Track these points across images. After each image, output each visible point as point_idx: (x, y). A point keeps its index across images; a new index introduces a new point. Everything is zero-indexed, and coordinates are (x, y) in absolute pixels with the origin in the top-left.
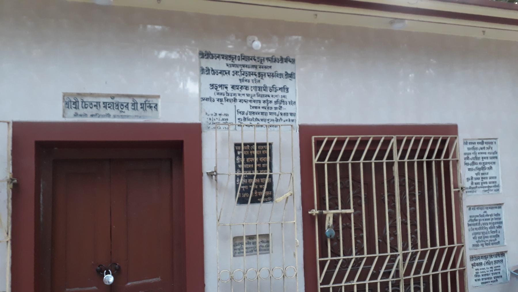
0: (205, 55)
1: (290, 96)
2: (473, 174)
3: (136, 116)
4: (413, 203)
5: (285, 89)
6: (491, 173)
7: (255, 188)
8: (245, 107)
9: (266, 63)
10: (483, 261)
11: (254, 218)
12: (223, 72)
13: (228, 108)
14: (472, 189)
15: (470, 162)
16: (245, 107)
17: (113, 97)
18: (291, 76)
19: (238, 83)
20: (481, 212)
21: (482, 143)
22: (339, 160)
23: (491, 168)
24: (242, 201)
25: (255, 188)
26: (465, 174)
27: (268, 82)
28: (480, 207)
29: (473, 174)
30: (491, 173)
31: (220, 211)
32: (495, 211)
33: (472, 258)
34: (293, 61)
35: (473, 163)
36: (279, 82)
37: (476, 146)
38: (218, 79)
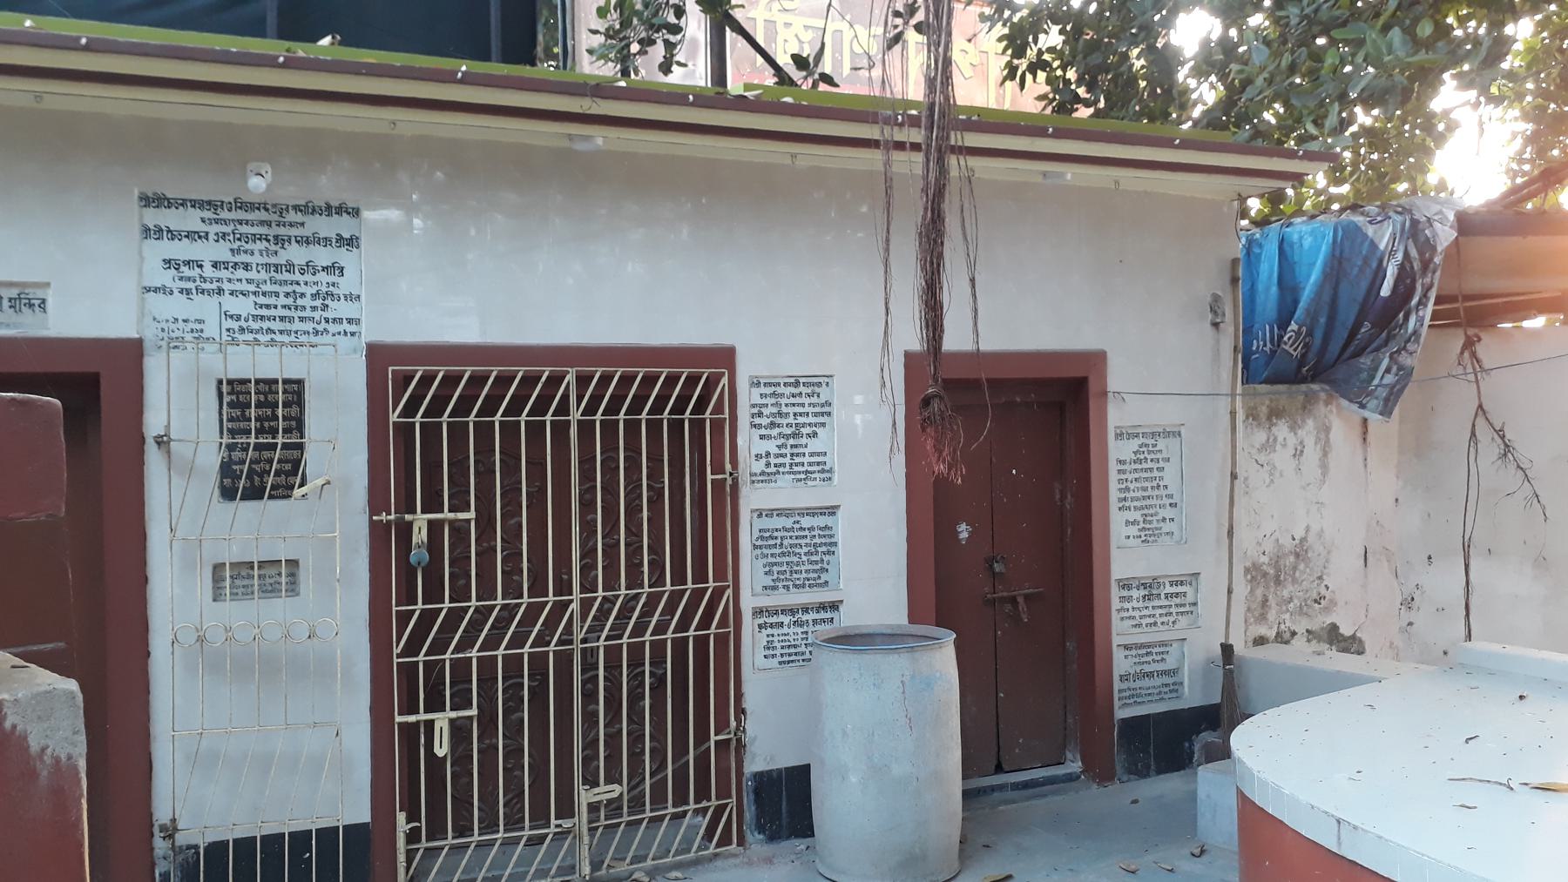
2: (771, 446)
5: (335, 269)
6: (814, 445)
8: (244, 306)
9: (292, 216)
10: (786, 619)
11: (255, 528)
12: (191, 235)
13: (206, 308)
14: (767, 477)
15: (765, 421)
16: (244, 306)
18: (351, 242)
19: (226, 256)
20: (788, 523)
21: (796, 384)
23: (815, 434)
26: (751, 444)
27: (296, 254)
28: (782, 512)
29: (771, 446)
31: (184, 519)
33: (758, 612)
34: (356, 212)
35: (773, 425)
36: (322, 256)
38: (181, 250)
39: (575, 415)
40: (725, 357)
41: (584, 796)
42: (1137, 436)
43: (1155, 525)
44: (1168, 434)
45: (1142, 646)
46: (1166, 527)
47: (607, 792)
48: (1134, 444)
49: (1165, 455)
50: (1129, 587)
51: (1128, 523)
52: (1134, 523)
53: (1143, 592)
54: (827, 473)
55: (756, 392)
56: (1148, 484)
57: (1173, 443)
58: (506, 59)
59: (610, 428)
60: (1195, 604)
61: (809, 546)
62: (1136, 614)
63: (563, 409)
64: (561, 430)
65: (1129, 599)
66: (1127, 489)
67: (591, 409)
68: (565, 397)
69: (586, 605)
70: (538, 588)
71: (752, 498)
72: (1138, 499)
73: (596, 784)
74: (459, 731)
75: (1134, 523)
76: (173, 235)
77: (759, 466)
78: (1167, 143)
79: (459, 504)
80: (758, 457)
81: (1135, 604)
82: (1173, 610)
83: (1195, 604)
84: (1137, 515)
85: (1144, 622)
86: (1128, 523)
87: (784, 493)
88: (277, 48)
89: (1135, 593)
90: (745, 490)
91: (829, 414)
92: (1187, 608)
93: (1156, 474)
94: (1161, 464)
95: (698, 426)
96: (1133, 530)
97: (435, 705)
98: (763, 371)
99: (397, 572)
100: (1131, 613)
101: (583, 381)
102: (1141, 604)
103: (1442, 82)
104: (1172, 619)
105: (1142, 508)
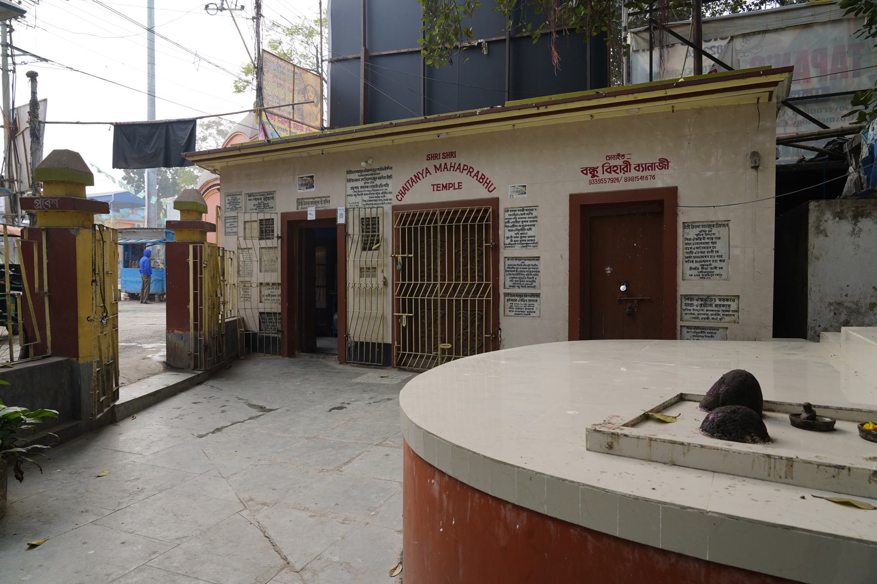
0: (349, 172)
1: (390, 189)
2: (513, 234)
3: (870, 459)
4: (443, 246)
5: (387, 185)
6: (530, 233)
7: (370, 242)
8: (366, 198)
9: (377, 172)
10: (518, 299)
11: (370, 258)
12: (357, 180)
13: (359, 199)
14: (511, 245)
15: (510, 224)
16: (366, 198)
17: (313, 198)
18: (390, 177)
19: (363, 185)
20: (520, 263)
21: (523, 210)
22: (414, 225)
23: (530, 229)
24: (364, 249)
25: (370, 242)
26: (505, 233)
27: (378, 182)
28: (517, 258)
29: (513, 234)
30: (530, 233)
31: (355, 258)
32: (533, 262)
33: (506, 295)
34: (391, 168)
35: (513, 226)
36: (384, 182)
37: (517, 212)
38: (354, 184)
39: (440, 224)
41: (441, 346)
42: (699, 226)
43: (709, 270)
44: (719, 225)
45: (698, 328)
46: (716, 272)
47: (448, 346)
49: (717, 236)
50: (692, 299)
51: (691, 268)
52: (695, 269)
54: (536, 245)
55: (507, 214)
56: (706, 250)
58: (365, 123)
59: (450, 228)
60: (737, 311)
61: (528, 271)
62: (696, 312)
63: (436, 222)
64: (435, 228)
65: (692, 305)
66: (692, 252)
67: (444, 222)
68: (436, 219)
69: (442, 285)
71: (504, 253)
72: (698, 257)
73: (444, 342)
74: (409, 319)
75: (695, 269)
76: (353, 180)
77: (508, 241)
78: (614, 94)
80: (508, 238)
81: (695, 308)
82: (720, 313)
83: (737, 311)
84: (698, 265)
85: (700, 317)
86: (691, 268)
87: (517, 251)
89: (695, 303)
90: (502, 250)
91: (273, 198)
92: (731, 313)
93: (710, 245)
94: (714, 240)
95: (480, 227)
96: (695, 272)
97: (404, 312)
98: (508, 205)
100: (692, 311)
101: (442, 213)
102: (699, 308)
104: (719, 317)
105: (701, 261)
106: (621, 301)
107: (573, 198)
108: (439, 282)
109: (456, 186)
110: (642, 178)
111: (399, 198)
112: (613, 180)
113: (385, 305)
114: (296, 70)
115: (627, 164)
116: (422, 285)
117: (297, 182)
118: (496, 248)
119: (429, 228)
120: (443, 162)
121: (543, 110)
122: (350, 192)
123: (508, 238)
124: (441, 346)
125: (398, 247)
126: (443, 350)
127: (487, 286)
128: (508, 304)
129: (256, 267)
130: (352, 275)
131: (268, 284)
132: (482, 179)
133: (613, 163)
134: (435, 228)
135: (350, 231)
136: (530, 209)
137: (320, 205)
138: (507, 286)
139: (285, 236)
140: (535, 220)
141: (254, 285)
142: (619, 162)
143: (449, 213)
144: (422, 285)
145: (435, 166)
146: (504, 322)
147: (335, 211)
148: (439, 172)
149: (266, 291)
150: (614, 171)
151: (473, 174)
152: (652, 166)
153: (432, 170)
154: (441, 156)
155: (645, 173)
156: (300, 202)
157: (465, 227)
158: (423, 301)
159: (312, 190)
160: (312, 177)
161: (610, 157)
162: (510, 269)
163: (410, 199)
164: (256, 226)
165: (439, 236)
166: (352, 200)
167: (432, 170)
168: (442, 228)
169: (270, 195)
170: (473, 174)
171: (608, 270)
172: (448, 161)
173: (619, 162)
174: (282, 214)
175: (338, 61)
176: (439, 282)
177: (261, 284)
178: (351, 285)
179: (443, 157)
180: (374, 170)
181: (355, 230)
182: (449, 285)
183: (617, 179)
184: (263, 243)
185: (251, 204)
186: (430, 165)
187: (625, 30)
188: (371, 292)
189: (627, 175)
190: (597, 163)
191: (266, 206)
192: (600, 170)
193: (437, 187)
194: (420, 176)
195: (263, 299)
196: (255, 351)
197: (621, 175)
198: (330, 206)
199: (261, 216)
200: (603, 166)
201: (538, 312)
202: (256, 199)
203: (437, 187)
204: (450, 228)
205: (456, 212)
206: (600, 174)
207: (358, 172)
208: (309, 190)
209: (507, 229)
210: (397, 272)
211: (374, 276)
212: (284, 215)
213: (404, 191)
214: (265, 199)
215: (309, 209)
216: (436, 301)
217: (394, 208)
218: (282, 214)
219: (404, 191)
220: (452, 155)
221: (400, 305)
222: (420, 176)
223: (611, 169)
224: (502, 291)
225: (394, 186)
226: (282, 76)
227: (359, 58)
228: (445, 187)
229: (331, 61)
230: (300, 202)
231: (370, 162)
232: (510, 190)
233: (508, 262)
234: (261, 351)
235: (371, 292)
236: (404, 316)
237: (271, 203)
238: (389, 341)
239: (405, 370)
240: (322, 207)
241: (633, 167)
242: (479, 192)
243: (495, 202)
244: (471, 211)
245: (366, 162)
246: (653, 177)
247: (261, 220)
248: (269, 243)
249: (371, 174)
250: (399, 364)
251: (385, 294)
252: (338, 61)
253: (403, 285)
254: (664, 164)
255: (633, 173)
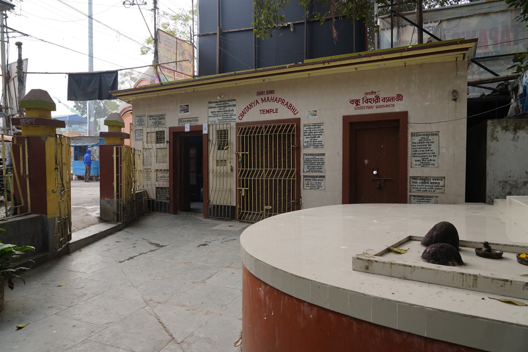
1: (234, 113)
2: (309, 140)
5: (233, 110)
6: (319, 139)
8: (220, 118)
9: (227, 102)
10: (312, 179)
11: (223, 154)
12: (215, 107)
13: (216, 119)
14: (307, 147)
15: (307, 134)
16: (220, 118)
18: (234, 105)
20: (313, 157)
21: (315, 125)
22: (249, 134)
24: (219, 149)
26: (303, 139)
27: (227, 109)
28: (311, 155)
29: (309, 140)
30: (319, 139)
31: (213, 154)
32: (321, 157)
33: (304, 176)
34: (235, 100)
35: (309, 135)
36: (231, 108)
38: (213, 110)
39: (264, 134)
40: (345, 119)
41: (265, 207)
42: (421, 135)
43: (427, 161)
44: (433, 134)
45: (420, 196)
46: (431, 162)
48: (419, 138)
49: (432, 141)
51: (416, 161)
52: (419, 161)
53: (421, 181)
54: (322, 146)
55: (305, 128)
57: (435, 138)
59: (271, 136)
60: (444, 186)
61: (318, 162)
62: (419, 187)
63: (262, 133)
64: (262, 136)
65: (416, 183)
66: (416, 151)
67: (267, 132)
68: (263, 131)
70: (258, 167)
71: (303, 151)
72: (420, 154)
74: (246, 191)
75: (419, 161)
76: (212, 108)
79: (247, 151)
80: (306, 142)
81: (418, 184)
82: (434, 187)
83: (444, 186)
84: (420, 159)
85: (422, 190)
86: (416, 161)
87: (311, 150)
88: (356, 54)
89: (418, 181)
91: (164, 118)
92: (440, 187)
93: (428, 146)
94: (430, 144)
95: (289, 135)
96: (418, 163)
97: (243, 187)
99: (243, 162)
101: (266, 127)
102: (421, 184)
103: (33, 91)
104: (433, 190)
105: (422, 156)
106: (373, 180)
107: (345, 119)
108: (264, 169)
109: (275, 111)
110: (386, 106)
111: (240, 118)
112: (369, 107)
113: (232, 183)
114: (178, 41)
115: (378, 98)
116: (254, 171)
117: (179, 109)
118: (299, 148)
119: (258, 136)
120: (266, 96)
121: (326, 65)
122: (211, 114)
123: (306, 142)
124: (265, 207)
125: (239, 148)
126: (267, 210)
127: (293, 171)
128: (306, 182)
129: (154, 160)
130: (212, 164)
131: (161, 170)
132: (290, 107)
133: (369, 97)
134: (262, 136)
135: (211, 138)
136: (319, 125)
137: (192, 123)
138: (305, 171)
139: (172, 142)
140: (322, 131)
141: (153, 171)
142: (373, 96)
143: (270, 127)
144: (254, 171)
145: (262, 99)
146: (303, 193)
147: (202, 126)
148: (264, 103)
149: (160, 175)
150: (370, 102)
151: (284, 104)
152: (392, 99)
153: (260, 101)
154: (266, 93)
155: (388, 103)
156: (180, 120)
157: (280, 136)
158: (254, 180)
159: (188, 113)
160: (188, 106)
161: (367, 94)
162: (307, 161)
163: (247, 118)
164: (154, 135)
165: (264, 141)
166: (212, 119)
167: (260, 101)
168: (266, 136)
169: (162, 117)
170: (284, 104)
171: (366, 162)
172: (270, 96)
173: (373, 96)
174: (169, 128)
175: (203, 35)
176: (264, 169)
177: (157, 170)
178: (211, 171)
179: (266, 93)
180: (225, 101)
181: (213, 138)
182: (270, 171)
183: (372, 107)
184: (158, 145)
185: (151, 122)
186: (259, 98)
187: (376, 17)
188: (224, 175)
189: (378, 104)
190: (360, 97)
191: (160, 123)
192: (361, 101)
193: (263, 112)
194: (253, 105)
195: (158, 179)
196: (153, 210)
197: (374, 104)
198: (199, 123)
199: (157, 129)
200: (363, 99)
201: (323, 187)
202: (154, 119)
203: (263, 112)
204: (271, 136)
205: (274, 127)
206: (361, 104)
207: (215, 102)
208: (186, 113)
209: (305, 137)
210: (239, 163)
211: (225, 165)
212: (170, 129)
213: (243, 114)
214: (159, 119)
215: (186, 125)
216: (262, 180)
217: (237, 124)
218: (169, 128)
219: (243, 114)
220: (272, 92)
221: (241, 183)
222: (253, 105)
223: (368, 101)
224: (302, 174)
225: (237, 111)
226: (169, 45)
227: (216, 34)
228: (268, 112)
229: (199, 36)
230: (180, 120)
231: (222, 96)
232: (307, 113)
233: (306, 157)
234: (157, 211)
235: (224, 175)
236: (243, 189)
237: (163, 121)
238: (234, 204)
239: (243, 222)
240: (194, 123)
241: (381, 99)
242: (288, 115)
243: (298, 120)
244: (283, 126)
245: (220, 96)
246: (393, 105)
247: (157, 132)
248: (162, 145)
249: (223, 104)
250: (240, 218)
251: (232, 176)
252: (203, 35)
253: (242, 171)
254: (400, 97)
255: (381, 103)
